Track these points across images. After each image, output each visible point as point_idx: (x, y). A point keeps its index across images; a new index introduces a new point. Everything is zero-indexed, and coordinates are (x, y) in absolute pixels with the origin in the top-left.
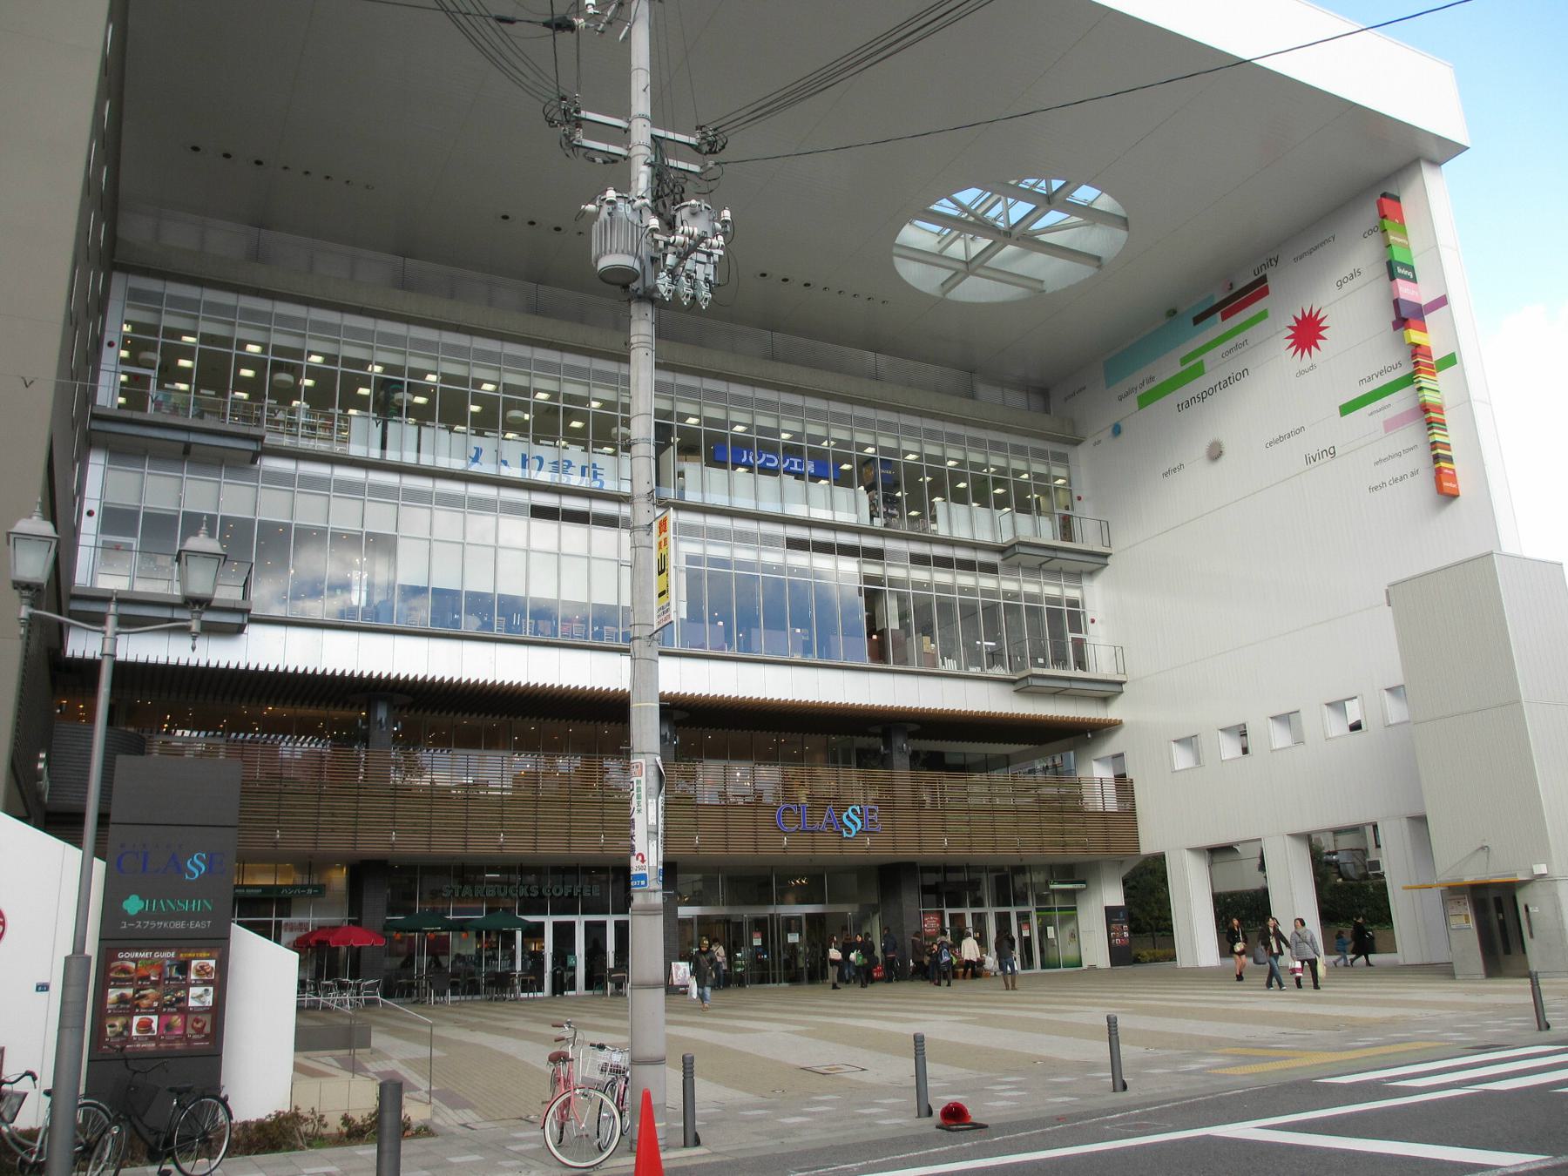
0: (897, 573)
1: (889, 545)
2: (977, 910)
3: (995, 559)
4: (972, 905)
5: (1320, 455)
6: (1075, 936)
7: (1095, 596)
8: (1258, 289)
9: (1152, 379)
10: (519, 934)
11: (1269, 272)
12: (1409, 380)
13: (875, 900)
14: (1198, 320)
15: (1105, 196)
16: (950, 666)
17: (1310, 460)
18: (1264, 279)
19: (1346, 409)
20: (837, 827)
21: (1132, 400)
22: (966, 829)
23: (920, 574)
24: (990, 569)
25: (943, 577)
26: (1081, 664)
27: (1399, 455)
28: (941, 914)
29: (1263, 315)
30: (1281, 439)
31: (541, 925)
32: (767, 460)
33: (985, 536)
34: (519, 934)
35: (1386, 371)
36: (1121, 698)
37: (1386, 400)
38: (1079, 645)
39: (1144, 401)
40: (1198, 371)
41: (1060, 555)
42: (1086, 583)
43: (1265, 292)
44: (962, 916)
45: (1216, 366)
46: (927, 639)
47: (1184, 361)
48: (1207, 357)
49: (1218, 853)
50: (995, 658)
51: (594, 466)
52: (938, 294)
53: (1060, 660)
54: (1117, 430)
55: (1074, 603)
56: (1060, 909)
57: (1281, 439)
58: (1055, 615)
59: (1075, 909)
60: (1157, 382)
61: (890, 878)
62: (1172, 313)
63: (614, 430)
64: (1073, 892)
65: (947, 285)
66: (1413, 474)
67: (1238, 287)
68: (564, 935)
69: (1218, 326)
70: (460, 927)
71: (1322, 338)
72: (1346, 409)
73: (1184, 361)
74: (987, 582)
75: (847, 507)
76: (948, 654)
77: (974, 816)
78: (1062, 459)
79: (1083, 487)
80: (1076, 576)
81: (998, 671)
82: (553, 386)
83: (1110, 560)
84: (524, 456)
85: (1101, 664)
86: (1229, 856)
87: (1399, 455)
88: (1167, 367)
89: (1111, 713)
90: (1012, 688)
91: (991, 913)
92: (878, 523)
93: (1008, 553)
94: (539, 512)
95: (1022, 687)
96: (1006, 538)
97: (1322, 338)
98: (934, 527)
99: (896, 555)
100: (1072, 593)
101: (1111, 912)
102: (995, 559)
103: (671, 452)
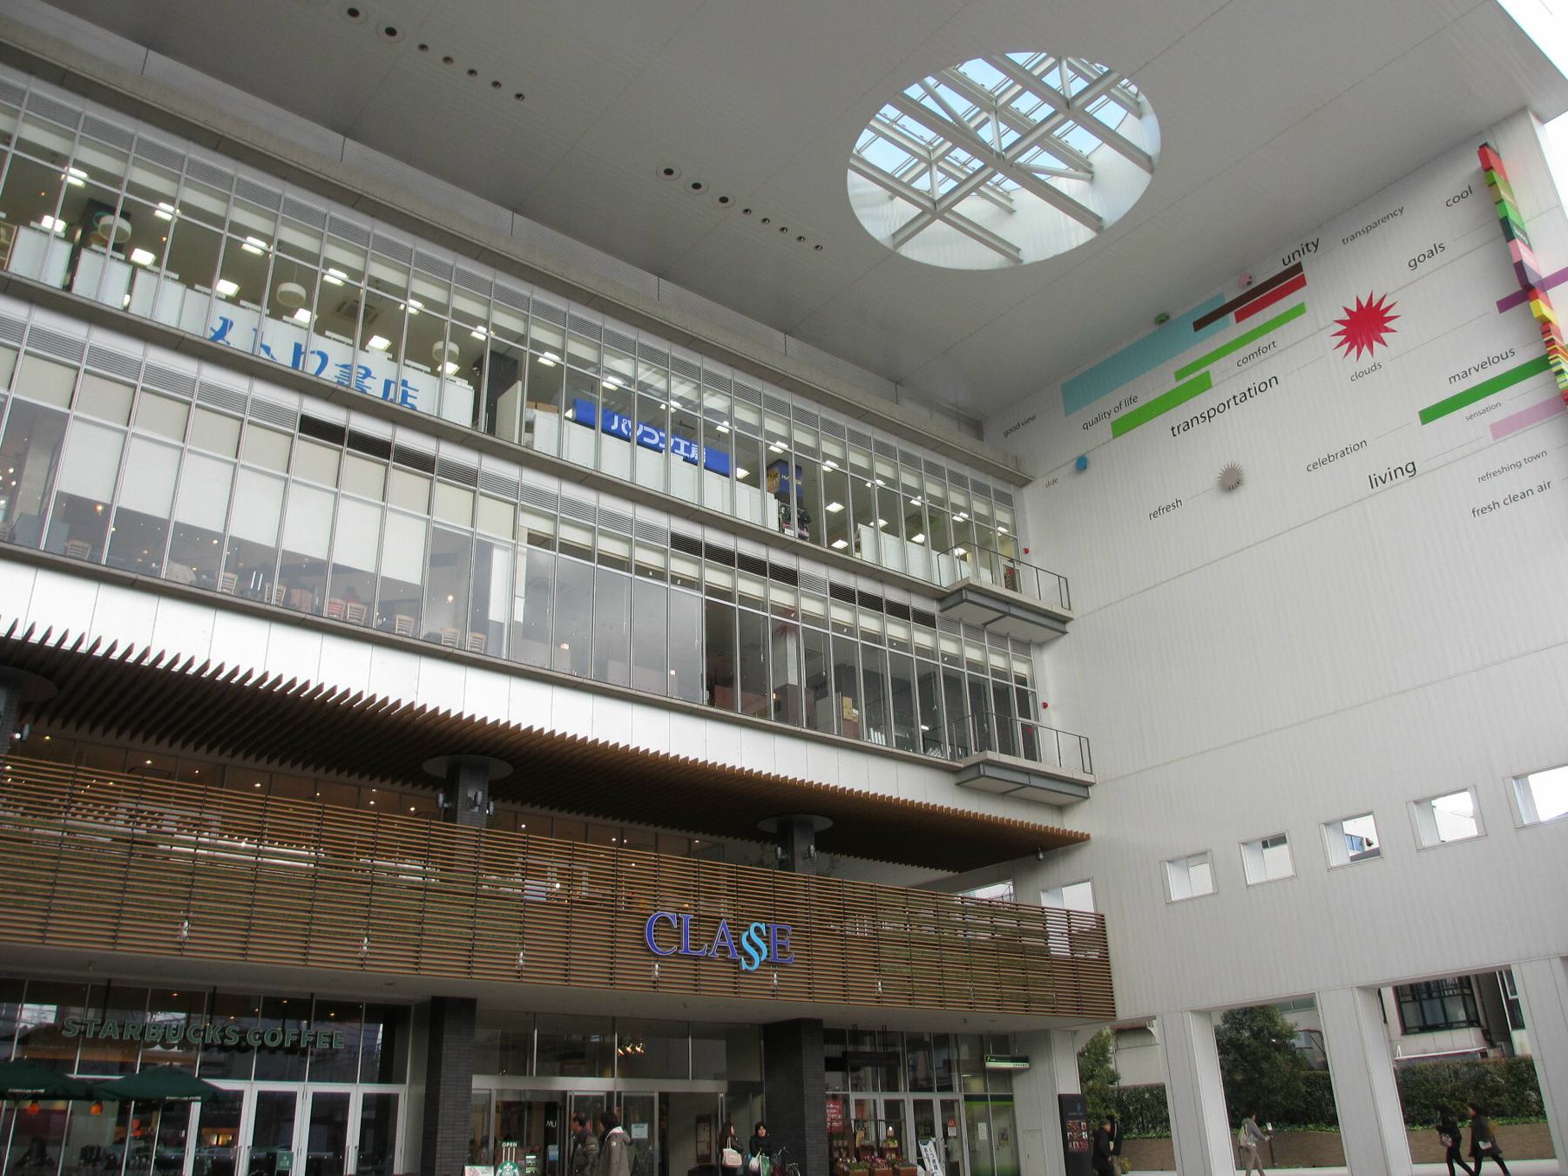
0: (811, 606)
1: (805, 567)
2: (947, 1096)
3: (931, 607)
4: (941, 1089)
5: (1393, 474)
6: (1008, 1137)
7: (1050, 673)
8: (1290, 279)
9: (1135, 399)
10: (196, 1109)
11: (1305, 260)
12: (1542, 364)
13: (755, 1075)
14: (1199, 325)
15: (1106, 147)
16: (877, 739)
17: (1374, 482)
18: (1299, 268)
19: (1428, 415)
20: (732, 958)
21: (1105, 426)
22: (906, 970)
23: (841, 614)
24: (926, 620)
25: (869, 622)
26: (1031, 754)
27: (1518, 465)
28: (846, 1100)
29: (1300, 310)
30: (1330, 458)
31: (238, 1096)
32: (646, 434)
33: (917, 572)
34: (196, 1109)
35: (1491, 361)
36: (1086, 805)
37: (1491, 399)
38: (1029, 732)
39: (1120, 428)
40: (1204, 384)
41: (1014, 611)
42: (1035, 655)
43: (1301, 282)
44: (288, 1101)
45: (1227, 378)
46: (847, 701)
47: (1180, 375)
48: (1214, 369)
49: (1422, 1003)
50: (932, 740)
51: (405, 383)
52: (889, 244)
53: (1008, 748)
54: (1082, 465)
55: (1021, 680)
56: (994, 1098)
57: (1330, 458)
58: (1002, 693)
59: (1010, 1098)
60: (1142, 402)
61: (783, 1041)
62: (1162, 319)
63: (439, 345)
64: (1008, 1074)
65: (909, 231)
66: (1541, 488)
67: (1260, 279)
68: (275, 1113)
69: (1230, 328)
70: (89, 1094)
71: (1371, 348)
72: (1428, 415)
73: (1180, 375)
74: (922, 638)
75: (755, 506)
76: (876, 723)
77: (917, 952)
78: (1005, 500)
79: (1032, 536)
80: (1024, 647)
81: (934, 755)
82: (354, 261)
83: (1069, 627)
84: (298, 347)
85: (1056, 755)
86: (1139, 1040)
87: (1518, 465)
88: (1156, 382)
89: (1072, 823)
90: (952, 780)
91: (908, 1098)
92: (791, 533)
93: (951, 601)
94: (311, 427)
95: (964, 778)
96: (944, 580)
97: (1387, 330)
98: (858, 555)
99: (813, 582)
100: (1020, 668)
101: (1066, 1104)
102: (931, 607)
103: (519, 390)
